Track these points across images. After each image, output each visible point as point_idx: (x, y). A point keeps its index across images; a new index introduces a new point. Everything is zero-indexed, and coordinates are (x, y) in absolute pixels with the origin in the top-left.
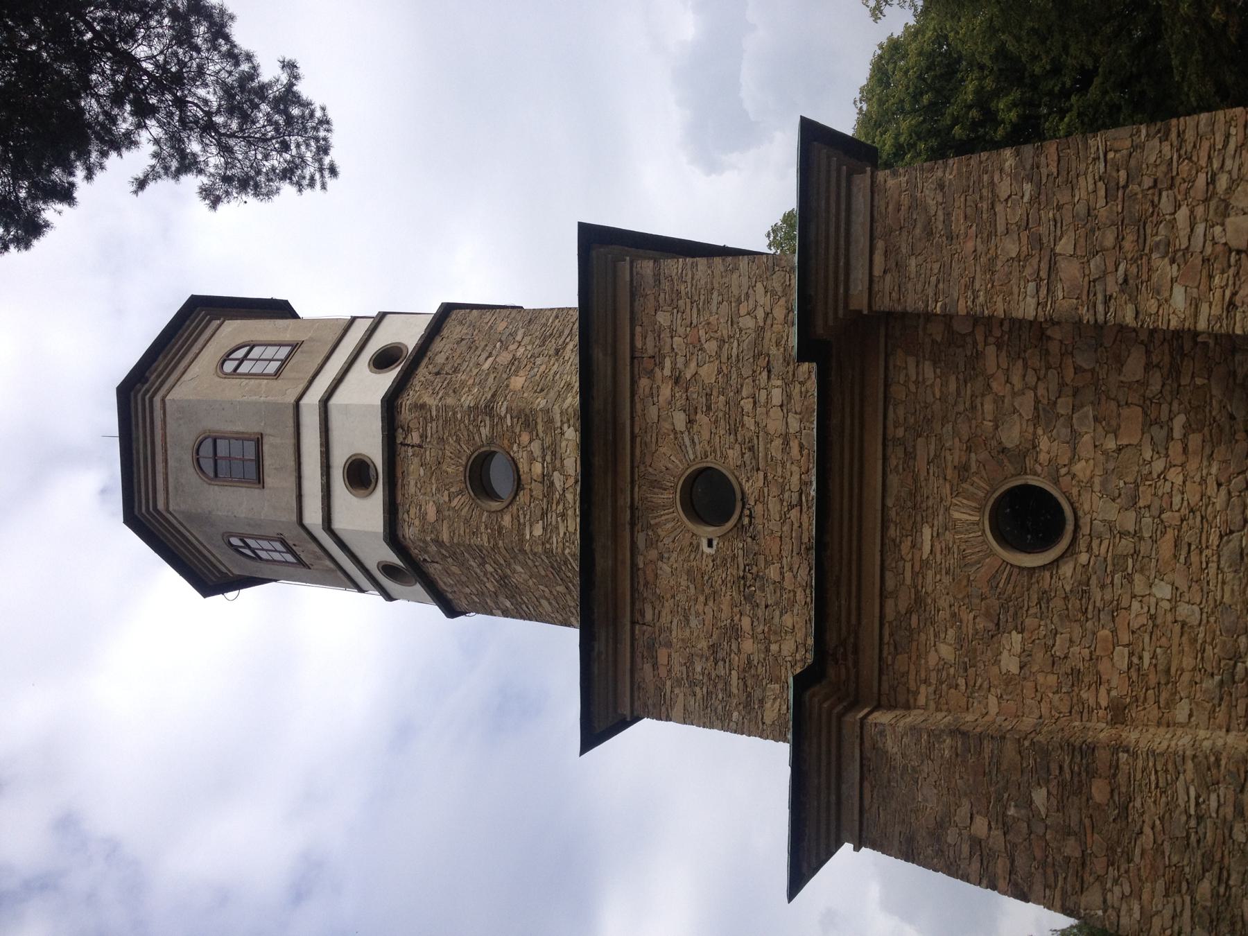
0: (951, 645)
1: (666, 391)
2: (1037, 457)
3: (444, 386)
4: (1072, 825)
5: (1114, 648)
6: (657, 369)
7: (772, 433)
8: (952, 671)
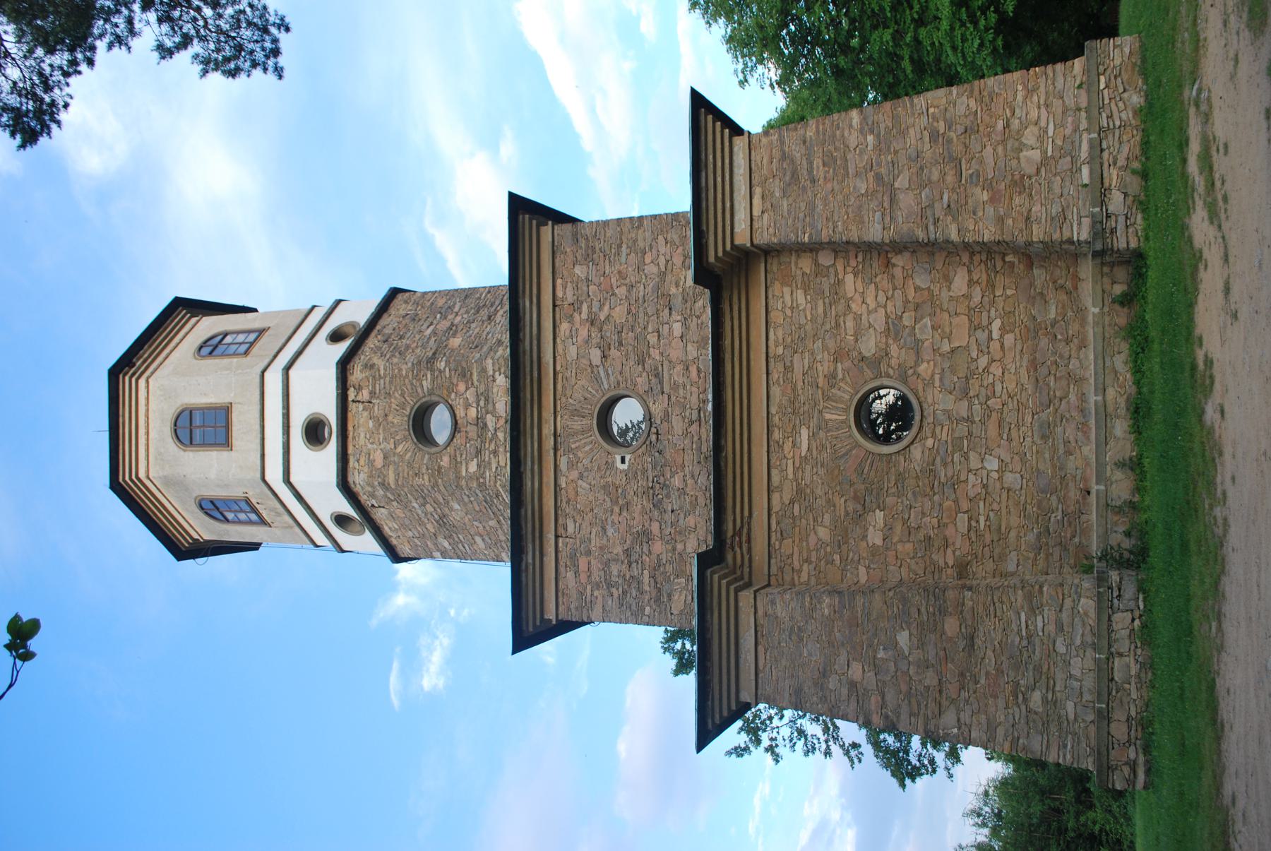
3: (391, 349)
4: (930, 658)
6: (576, 315)
8: (828, 549)
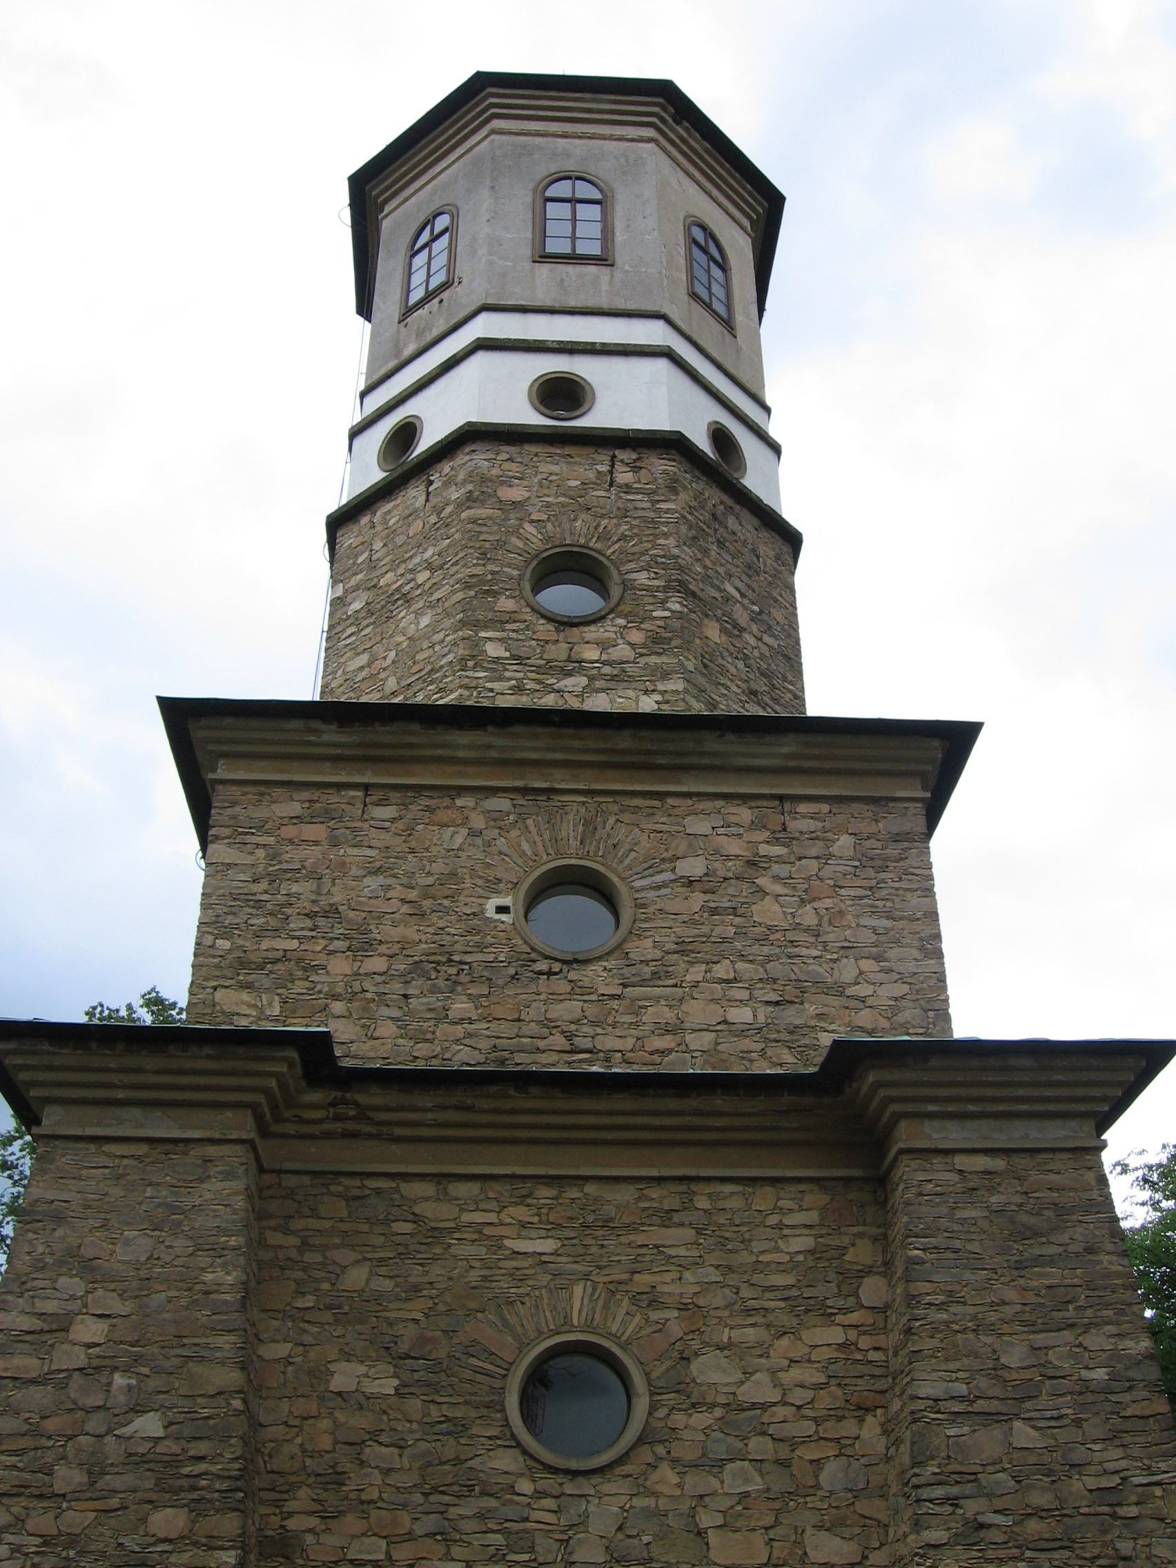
0: (367, 1282)
1: (734, 847)
2: (680, 1410)
4: (108, 1477)
5: (385, 1537)
7: (684, 1007)
8: (326, 1286)
